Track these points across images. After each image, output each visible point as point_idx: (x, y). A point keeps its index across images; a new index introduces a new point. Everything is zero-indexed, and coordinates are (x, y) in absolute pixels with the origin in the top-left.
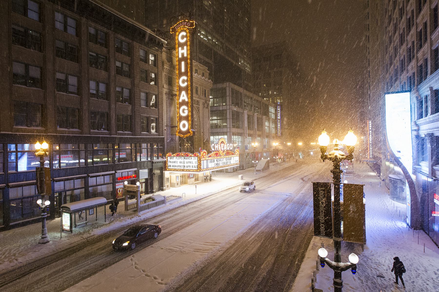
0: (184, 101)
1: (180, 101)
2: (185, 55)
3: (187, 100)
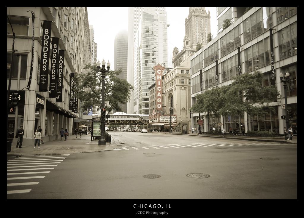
0: (159, 96)
1: (158, 96)
2: (160, 79)
3: (161, 96)
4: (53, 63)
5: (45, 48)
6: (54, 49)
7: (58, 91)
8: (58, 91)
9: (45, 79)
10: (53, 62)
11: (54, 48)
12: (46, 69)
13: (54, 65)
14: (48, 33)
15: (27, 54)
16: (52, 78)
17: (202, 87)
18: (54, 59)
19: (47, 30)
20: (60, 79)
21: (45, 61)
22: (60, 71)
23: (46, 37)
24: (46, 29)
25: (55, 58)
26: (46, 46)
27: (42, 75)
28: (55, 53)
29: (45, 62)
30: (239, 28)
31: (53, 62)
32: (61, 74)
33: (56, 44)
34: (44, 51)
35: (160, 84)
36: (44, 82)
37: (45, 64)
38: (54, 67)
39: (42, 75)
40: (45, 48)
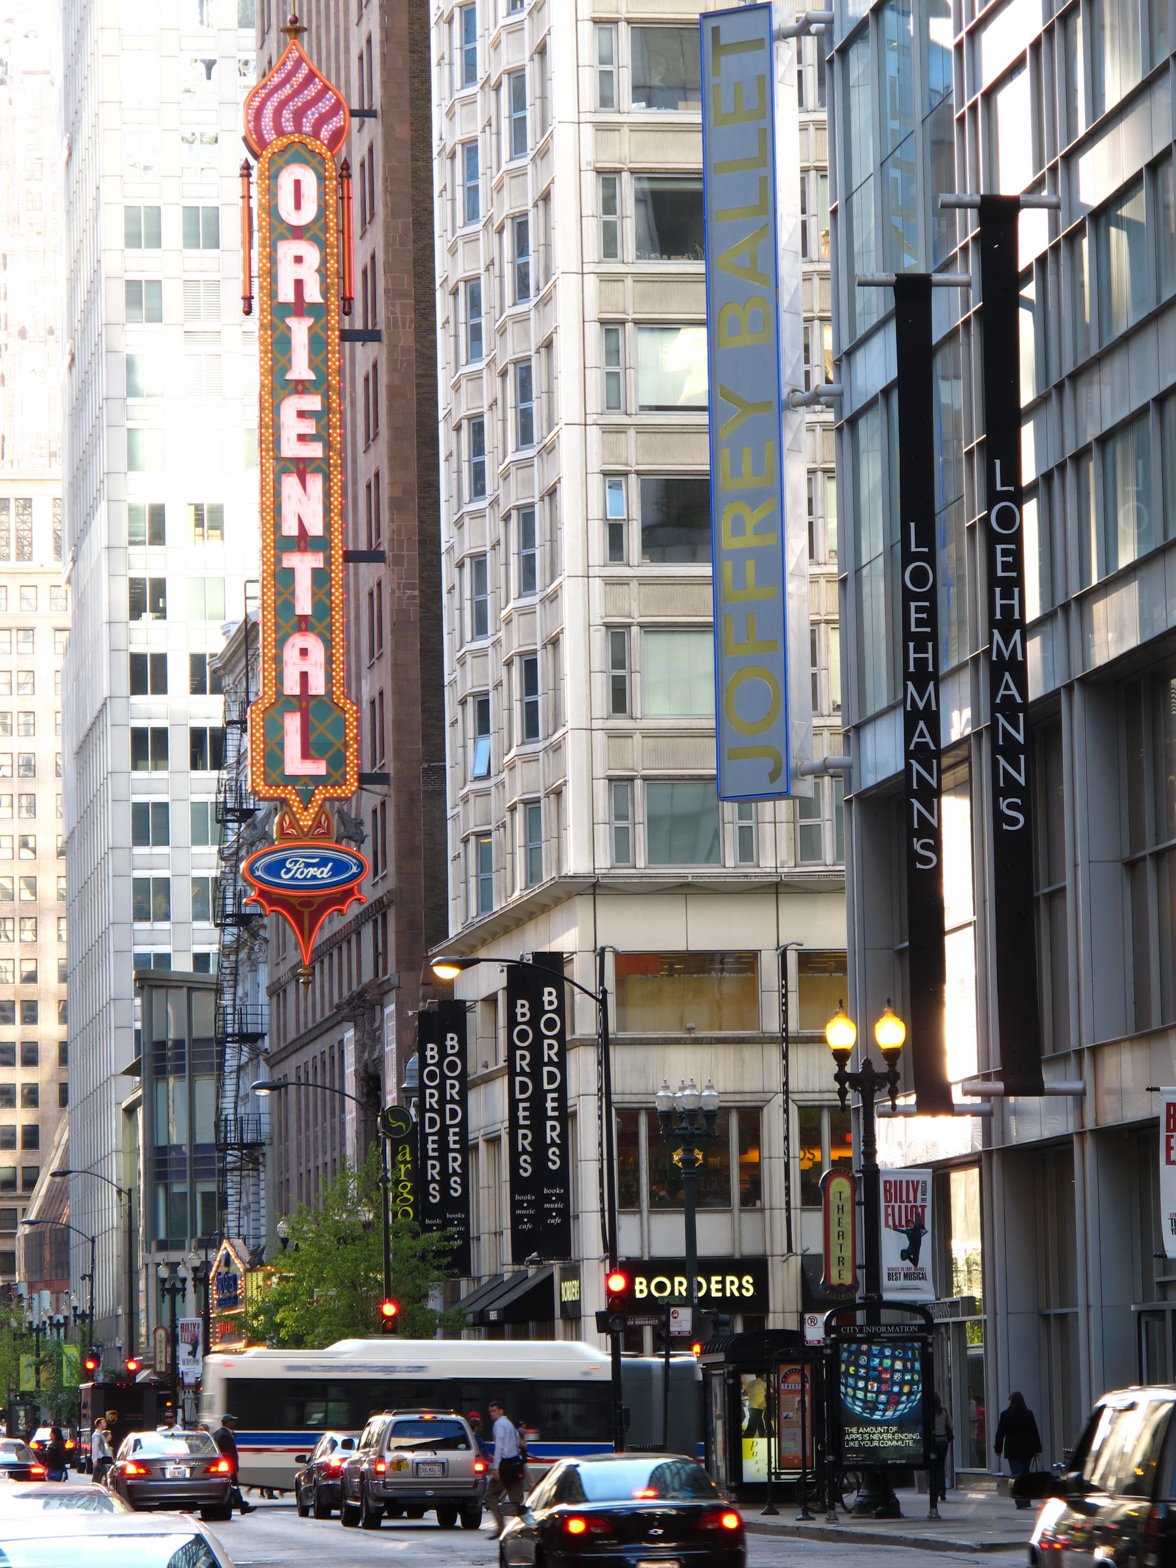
4: (448, 1122)
5: (549, 1072)
6: (457, 1072)
7: (548, 1198)
8: (548, 1198)
9: (561, 1206)
10: (549, 1083)
11: (520, 1019)
12: (530, 1169)
13: (525, 1109)
14: (554, 1006)
15: (761, 1108)
16: (521, 1171)
17: (350, 307)
18: (429, 1111)
19: (550, 994)
20: (553, 1128)
21: (455, 1160)
22: (521, 1092)
23: (550, 1024)
24: (520, 1002)
25: (527, 1070)
26: (432, 1109)
27: (517, 1197)
28: (433, 1084)
29: (456, 1165)
30: (1073, 171)
31: (549, 1083)
32: (457, 1130)
33: (455, 1036)
34: (518, 1096)
35: (315, 605)
36: (554, 1217)
37: (455, 1173)
38: (525, 1118)
39: (517, 1197)
40: (549, 1072)
